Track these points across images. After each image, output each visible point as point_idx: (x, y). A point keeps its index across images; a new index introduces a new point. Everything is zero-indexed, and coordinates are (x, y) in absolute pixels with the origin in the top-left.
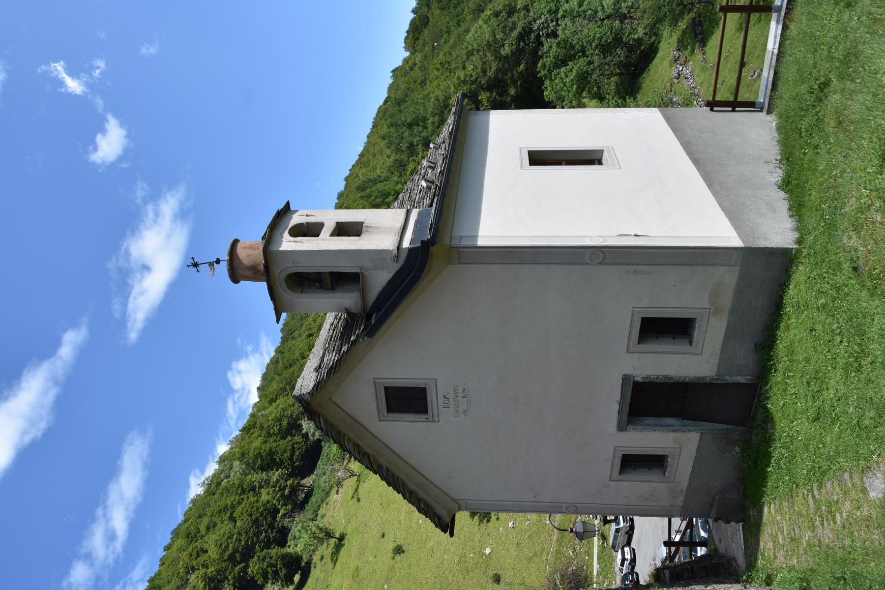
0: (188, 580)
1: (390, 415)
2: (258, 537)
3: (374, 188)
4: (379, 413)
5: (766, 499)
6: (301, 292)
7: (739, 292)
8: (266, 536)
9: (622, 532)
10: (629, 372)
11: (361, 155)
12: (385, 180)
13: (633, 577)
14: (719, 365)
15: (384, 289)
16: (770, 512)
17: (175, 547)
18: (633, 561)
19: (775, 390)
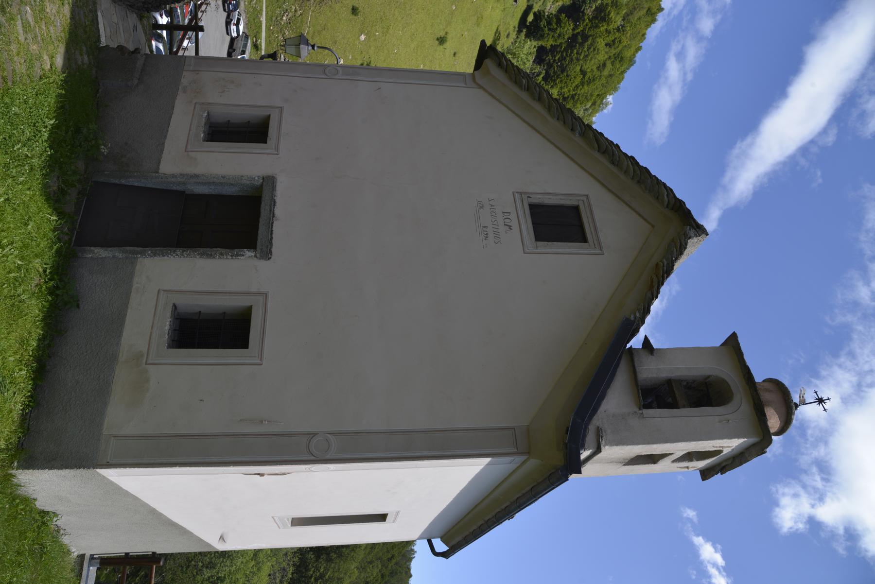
0: (623, 20)
1: (576, 203)
2: (562, 56)
4: (590, 205)
5: (59, 78)
6: (709, 376)
7: (103, 392)
8: (555, 56)
9: (239, 51)
10: (262, 264)
13: (229, 7)
14: (132, 274)
15: (608, 386)
16: (52, 57)
17: (633, 49)
18: (228, 23)
19: (44, 244)
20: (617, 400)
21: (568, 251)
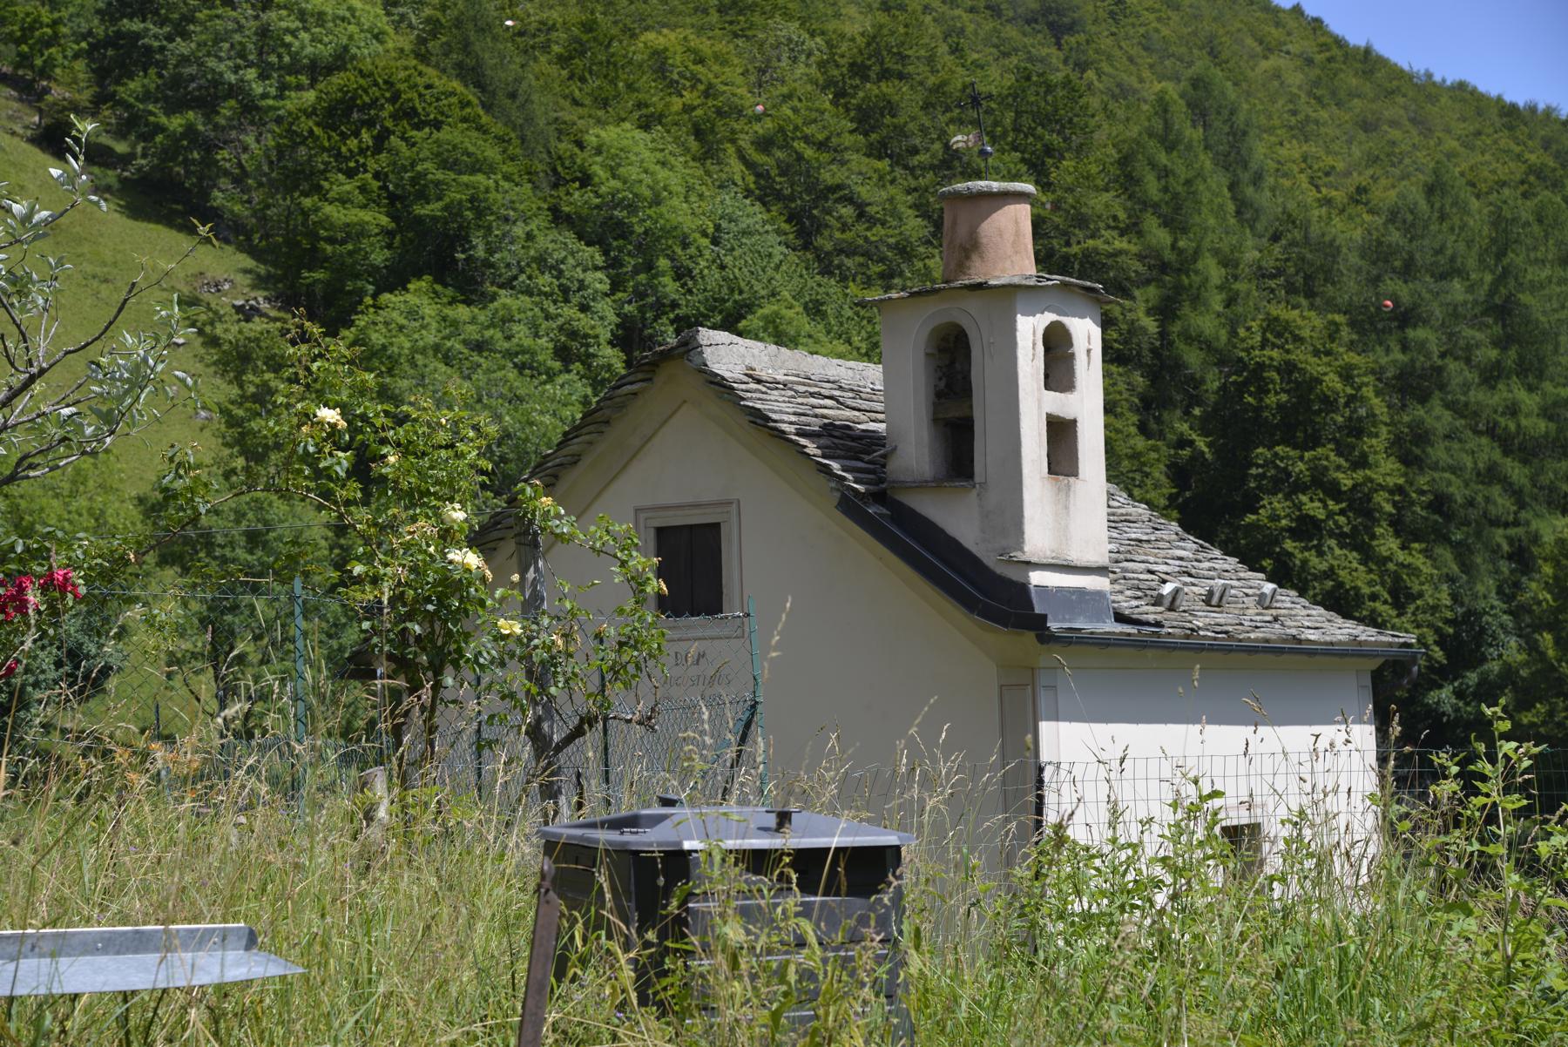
1: (652, 534)
3: (1206, 161)
11: (1367, 61)
12: (1242, 206)
20: (959, 519)
21: (735, 548)
